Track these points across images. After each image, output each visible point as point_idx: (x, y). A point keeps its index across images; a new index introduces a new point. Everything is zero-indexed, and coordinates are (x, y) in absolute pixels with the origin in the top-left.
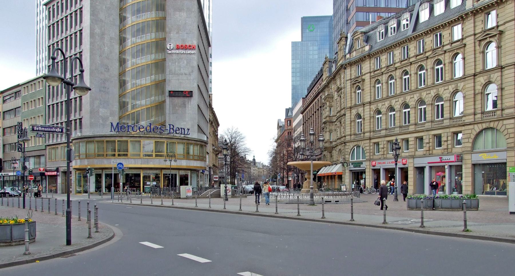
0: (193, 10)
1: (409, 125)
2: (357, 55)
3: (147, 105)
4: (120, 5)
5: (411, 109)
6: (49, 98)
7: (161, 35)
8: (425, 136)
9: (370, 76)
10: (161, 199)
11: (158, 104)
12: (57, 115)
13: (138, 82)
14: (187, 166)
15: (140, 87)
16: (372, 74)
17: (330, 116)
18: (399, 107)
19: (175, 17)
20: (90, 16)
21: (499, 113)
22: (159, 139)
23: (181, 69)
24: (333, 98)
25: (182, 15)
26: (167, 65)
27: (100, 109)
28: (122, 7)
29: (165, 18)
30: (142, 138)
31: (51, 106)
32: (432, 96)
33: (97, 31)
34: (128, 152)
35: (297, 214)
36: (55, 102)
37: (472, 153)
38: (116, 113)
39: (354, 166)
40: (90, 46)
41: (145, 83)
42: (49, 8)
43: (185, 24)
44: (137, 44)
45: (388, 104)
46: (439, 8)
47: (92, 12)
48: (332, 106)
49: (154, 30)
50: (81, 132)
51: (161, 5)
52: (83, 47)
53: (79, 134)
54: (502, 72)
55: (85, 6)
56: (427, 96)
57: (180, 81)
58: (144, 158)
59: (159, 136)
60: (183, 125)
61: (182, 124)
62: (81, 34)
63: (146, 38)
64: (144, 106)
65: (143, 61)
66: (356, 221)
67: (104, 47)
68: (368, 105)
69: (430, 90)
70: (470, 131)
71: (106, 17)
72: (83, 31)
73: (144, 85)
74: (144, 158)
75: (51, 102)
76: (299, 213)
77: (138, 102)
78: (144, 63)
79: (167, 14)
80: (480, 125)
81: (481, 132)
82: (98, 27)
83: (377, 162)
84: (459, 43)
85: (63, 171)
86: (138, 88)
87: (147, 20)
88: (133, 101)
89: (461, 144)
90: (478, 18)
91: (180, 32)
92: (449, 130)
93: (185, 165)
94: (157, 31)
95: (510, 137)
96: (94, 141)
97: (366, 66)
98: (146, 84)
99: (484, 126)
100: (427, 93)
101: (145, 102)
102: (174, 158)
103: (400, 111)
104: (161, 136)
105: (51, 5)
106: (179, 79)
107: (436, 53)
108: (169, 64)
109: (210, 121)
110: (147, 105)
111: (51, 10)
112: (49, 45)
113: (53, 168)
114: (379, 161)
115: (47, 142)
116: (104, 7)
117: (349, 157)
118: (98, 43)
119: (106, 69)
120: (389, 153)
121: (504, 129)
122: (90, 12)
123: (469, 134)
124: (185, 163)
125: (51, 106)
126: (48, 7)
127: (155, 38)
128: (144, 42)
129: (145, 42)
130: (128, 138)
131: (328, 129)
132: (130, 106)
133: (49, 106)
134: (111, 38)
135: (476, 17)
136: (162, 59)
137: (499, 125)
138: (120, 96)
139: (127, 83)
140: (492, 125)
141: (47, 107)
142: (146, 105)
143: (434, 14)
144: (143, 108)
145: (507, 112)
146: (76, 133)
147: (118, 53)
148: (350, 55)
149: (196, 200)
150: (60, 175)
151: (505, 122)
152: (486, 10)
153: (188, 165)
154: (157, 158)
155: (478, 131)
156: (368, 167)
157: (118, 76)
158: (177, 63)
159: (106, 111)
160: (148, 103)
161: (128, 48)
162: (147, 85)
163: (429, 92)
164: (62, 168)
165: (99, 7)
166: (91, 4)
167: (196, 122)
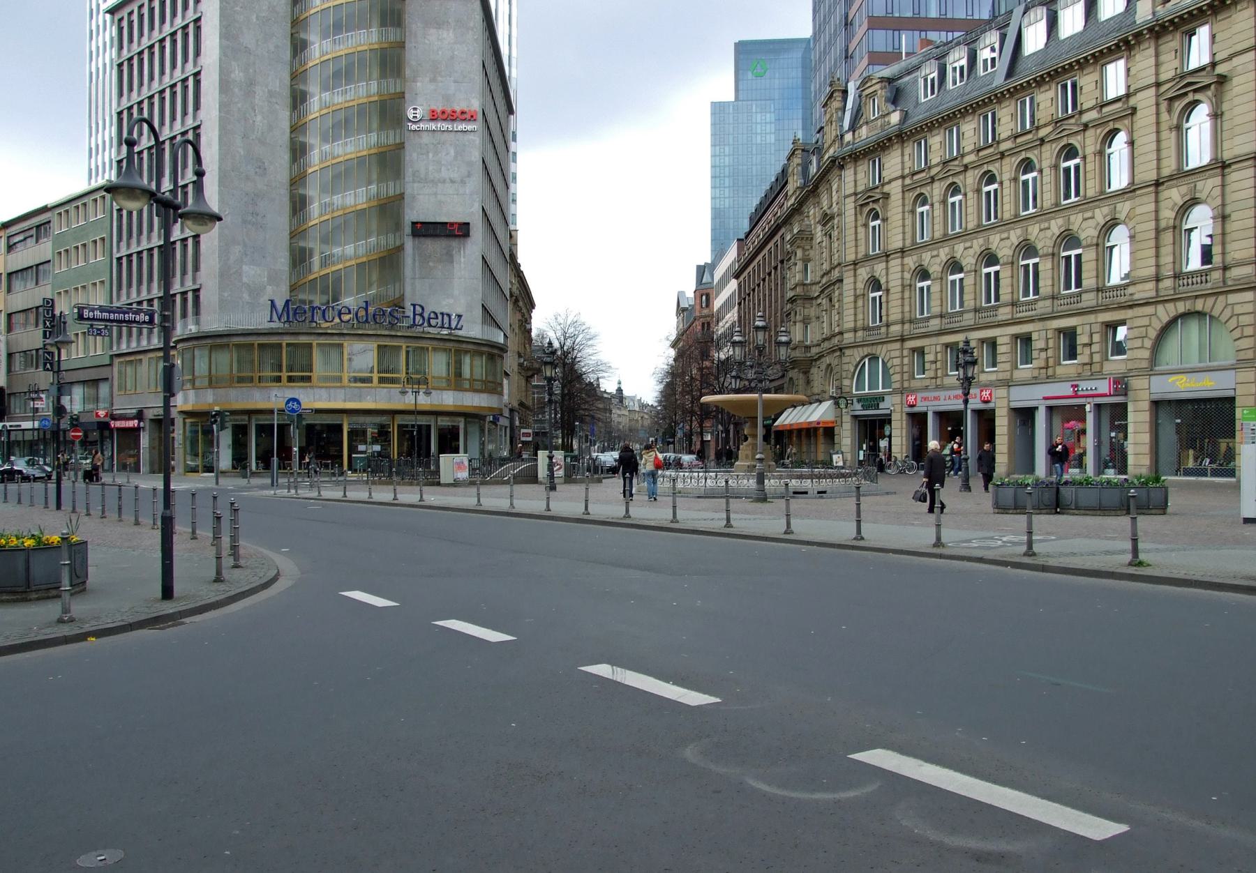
0: (472, 24)
1: (999, 307)
2: (870, 134)
3: (359, 258)
4: (293, 11)
5: (1001, 265)
7: (392, 86)
8: (1037, 333)
9: (903, 186)
13: (337, 199)
15: (341, 213)
16: (908, 181)
17: (804, 285)
19: (427, 41)
21: (1217, 275)
22: (388, 339)
24: (812, 239)
26: (407, 158)
28: (297, 18)
29: (401, 45)
30: (347, 338)
33: (237, 75)
36: (134, 249)
37: (1150, 375)
39: (862, 406)
40: (220, 112)
42: (121, 20)
43: (452, 58)
44: (334, 108)
46: (1072, 21)
47: (224, 30)
48: (809, 260)
49: (376, 74)
50: (197, 323)
52: (202, 114)
53: (193, 328)
54: (1223, 176)
55: (208, 14)
56: (1042, 235)
58: (351, 387)
59: (387, 333)
60: (446, 305)
62: (197, 83)
64: (351, 259)
67: (253, 114)
70: (1145, 321)
71: (257, 41)
72: (203, 76)
74: (351, 387)
76: (728, 519)
77: (337, 250)
78: (351, 153)
80: (1170, 306)
81: (1172, 322)
82: (238, 65)
83: (920, 395)
84: (1119, 105)
85: (153, 418)
86: (336, 214)
87: (359, 49)
88: (325, 247)
90: (1165, 43)
91: (439, 79)
92: (1096, 318)
93: (451, 404)
94: (383, 75)
95: (1245, 335)
98: (356, 206)
99: (1181, 307)
100: (1042, 227)
102: (425, 387)
103: (976, 271)
105: (124, 13)
106: (436, 194)
109: (511, 295)
111: (125, 24)
113: (129, 411)
114: (926, 394)
115: (115, 348)
116: (254, 18)
117: (852, 384)
118: (239, 105)
119: (257, 170)
121: (1230, 315)
122: (220, 29)
123: (1144, 329)
124: (452, 399)
126: (117, 17)
128: (351, 104)
129: (354, 103)
130: (312, 338)
131: (800, 315)
132: (316, 259)
133: (119, 259)
134: (271, 94)
136: (396, 144)
137: (1217, 306)
140: (1199, 305)
141: (115, 261)
142: (356, 257)
146: (185, 326)
147: (289, 131)
148: (854, 134)
149: (478, 490)
150: (147, 427)
151: (1232, 298)
152: (1185, 24)
153: (459, 404)
154: (382, 385)
155: (1165, 319)
156: (898, 408)
160: (361, 251)
161: (313, 116)
162: (359, 208)
163: (1046, 225)
164: (151, 410)
165: (242, 17)
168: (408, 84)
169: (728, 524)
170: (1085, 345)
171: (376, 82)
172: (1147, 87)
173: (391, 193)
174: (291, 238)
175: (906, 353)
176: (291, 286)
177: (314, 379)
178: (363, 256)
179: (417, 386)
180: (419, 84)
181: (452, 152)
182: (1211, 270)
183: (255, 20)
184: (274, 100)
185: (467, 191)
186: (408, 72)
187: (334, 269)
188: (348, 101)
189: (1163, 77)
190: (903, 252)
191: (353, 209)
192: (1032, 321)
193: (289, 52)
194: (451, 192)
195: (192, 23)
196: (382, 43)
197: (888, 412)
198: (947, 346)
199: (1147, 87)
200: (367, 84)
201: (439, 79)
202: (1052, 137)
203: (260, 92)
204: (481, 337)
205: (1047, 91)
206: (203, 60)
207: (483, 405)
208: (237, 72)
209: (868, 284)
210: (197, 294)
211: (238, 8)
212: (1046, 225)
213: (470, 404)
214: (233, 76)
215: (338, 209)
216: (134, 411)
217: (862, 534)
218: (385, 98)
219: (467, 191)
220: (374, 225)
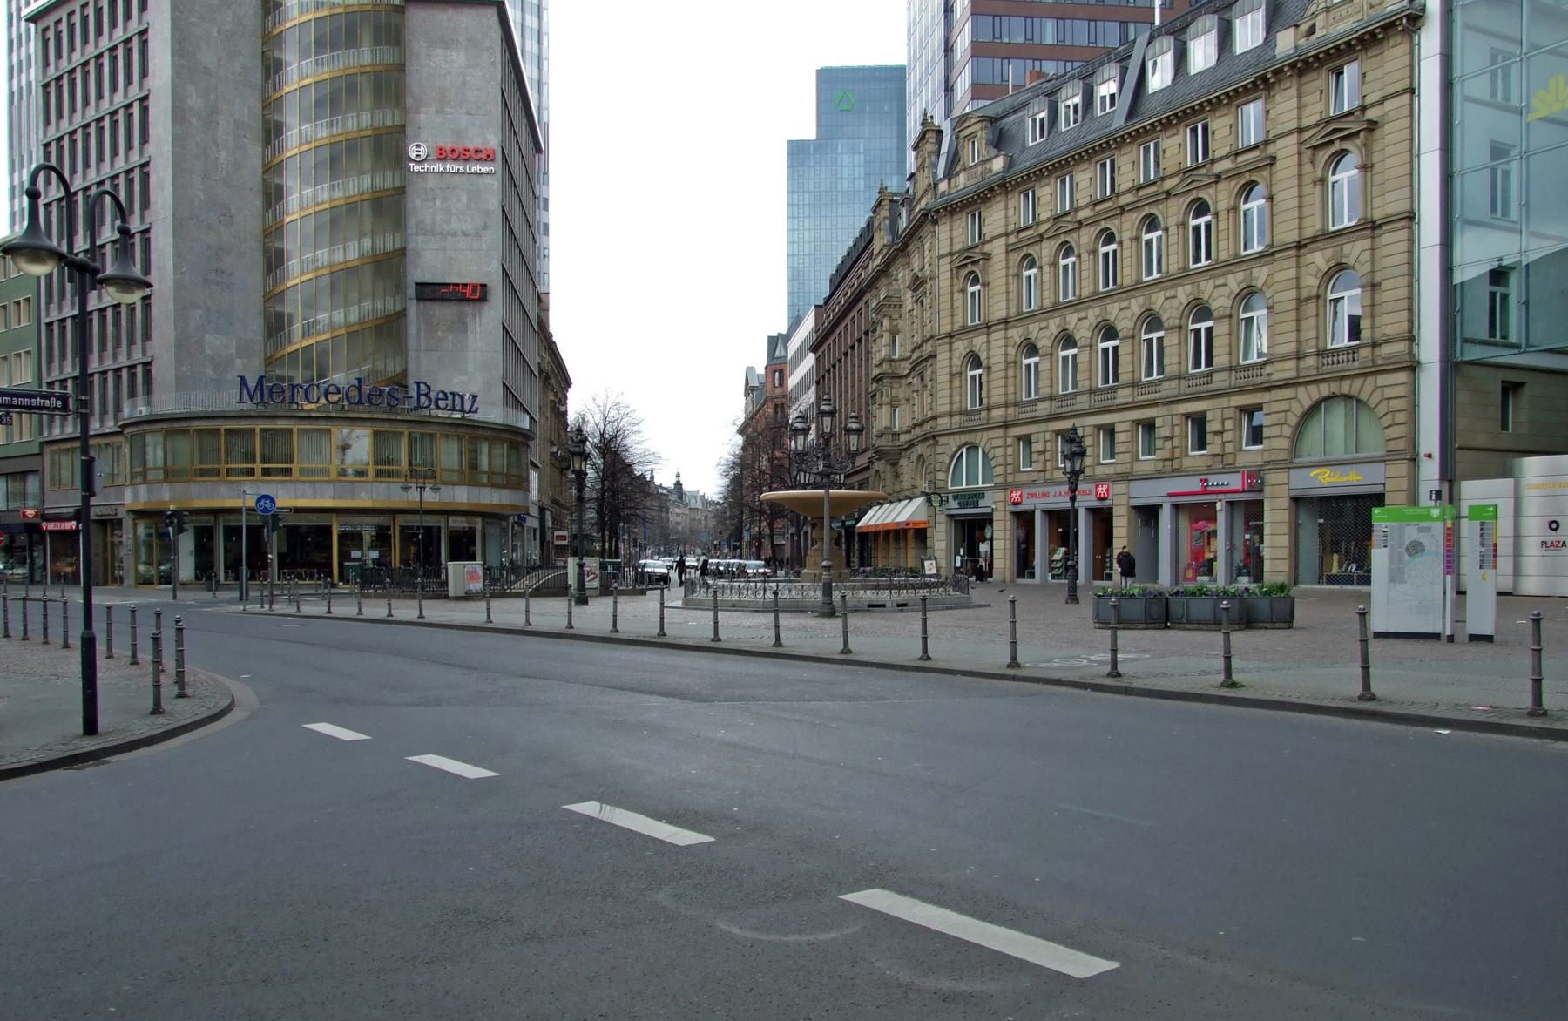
9: (1007, 245)
14: (470, 504)
16: (1012, 239)
17: (893, 360)
18: (1228, 303)
26: (409, 206)
30: (335, 423)
32: (1232, 292)
39: (959, 504)
42: (46, 30)
45: (1328, 261)
50: (149, 403)
53: (143, 410)
54: (1298, 256)
56: (1167, 304)
67: (215, 149)
68: (1000, 330)
69: (1128, 298)
70: (1284, 406)
71: (219, 60)
80: (1313, 389)
81: (1314, 409)
83: (1026, 491)
89: (1261, 443)
91: (448, 110)
92: (1229, 401)
93: (465, 501)
95: (1396, 422)
97: (997, 217)
99: (1325, 390)
101: (342, 315)
103: (1091, 346)
105: (50, 21)
107: (1193, 181)
109: (541, 371)
111: (51, 35)
113: (65, 511)
120: (1022, 469)
124: (465, 496)
126: (42, 25)
131: (887, 396)
133: (50, 325)
135: (1304, 80)
136: (394, 189)
141: (43, 327)
143: (1231, 46)
145: (995, 413)
146: (134, 407)
147: (260, 170)
148: (949, 183)
153: (476, 501)
155: (1307, 403)
156: (1000, 506)
163: (1172, 293)
170: (1216, 433)
172: (1288, 133)
175: (1009, 441)
180: (422, 116)
181: (465, 199)
182: (1358, 347)
189: (1306, 122)
190: (1006, 322)
192: (1156, 405)
197: (989, 510)
198: (1057, 433)
199: (1288, 133)
201: (448, 110)
202: (1180, 190)
205: (1174, 135)
208: (194, 98)
209: (1323, 285)
212: (1172, 293)
214: (189, 102)
215: (323, 267)
216: (72, 510)
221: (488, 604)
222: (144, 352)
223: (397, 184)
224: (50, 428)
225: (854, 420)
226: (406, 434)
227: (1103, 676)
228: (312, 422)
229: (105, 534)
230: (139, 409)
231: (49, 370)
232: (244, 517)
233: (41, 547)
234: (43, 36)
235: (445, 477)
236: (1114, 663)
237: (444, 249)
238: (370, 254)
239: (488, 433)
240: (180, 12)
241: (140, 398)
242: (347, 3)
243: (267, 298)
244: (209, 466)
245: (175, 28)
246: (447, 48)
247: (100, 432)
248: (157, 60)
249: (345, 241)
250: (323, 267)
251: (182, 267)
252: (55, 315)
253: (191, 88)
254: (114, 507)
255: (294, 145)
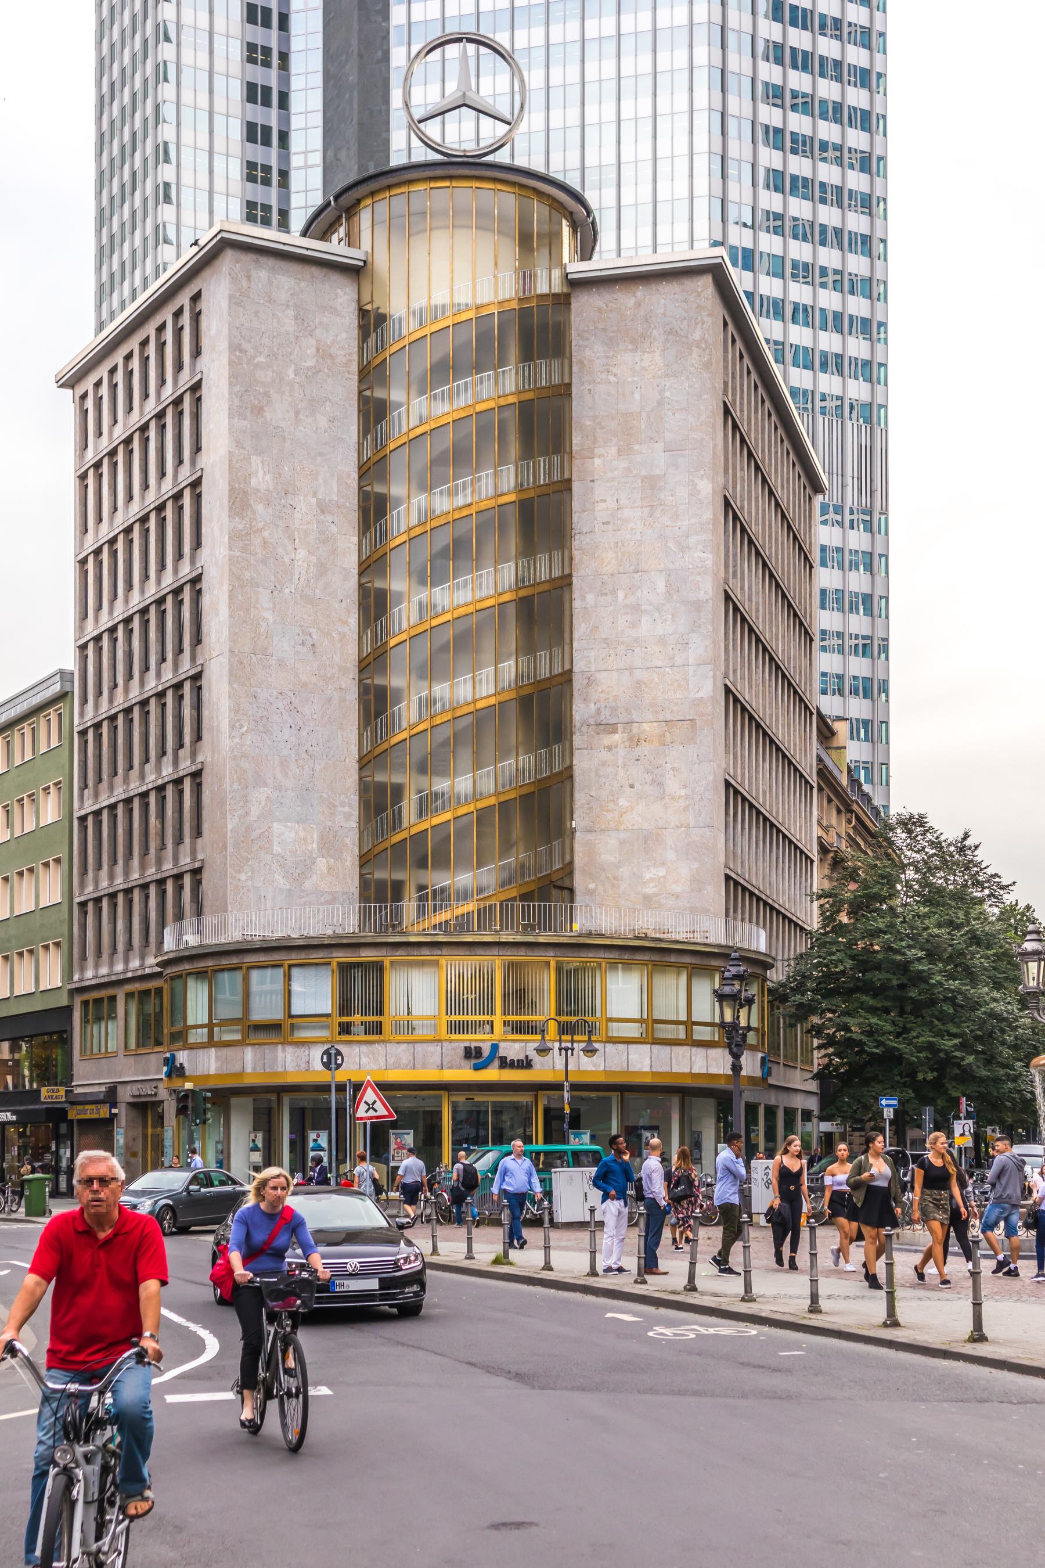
0: (697, 335)
3: (482, 798)
4: (361, 349)
6: (84, 786)
7: (543, 472)
10: (462, 1231)
11: (531, 789)
12: (114, 861)
13: (441, 690)
14: (654, 1074)
15: (448, 716)
19: (612, 378)
20: (231, 416)
22: (522, 951)
23: (643, 620)
25: (646, 364)
26: (577, 604)
27: (275, 825)
28: (369, 363)
29: (564, 391)
30: (445, 951)
31: (90, 819)
33: (261, 479)
34: (380, 1012)
35: (809, 1302)
36: (105, 801)
38: (348, 841)
40: (231, 549)
41: (469, 698)
42: (84, 397)
43: (660, 403)
44: (435, 524)
47: (237, 402)
49: (514, 448)
50: (199, 932)
51: (544, 327)
52: (205, 554)
53: (191, 939)
55: (211, 376)
57: (638, 673)
58: (451, 1041)
59: (519, 938)
60: (652, 880)
61: (648, 876)
62: (197, 498)
63: (473, 492)
64: (467, 802)
65: (464, 596)
66: (994, 1342)
67: (290, 547)
71: (297, 413)
72: (205, 488)
73: (468, 704)
74: (451, 1041)
75: (91, 802)
76: (814, 1298)
77: (441, 785)
78: (466, 605)
79: (575, 369)
82: (263, 463)
85: (131, 1100)
86: (438, 720)
87: (479, 408)
88: (424, 781)
91: (637, 447)
93: (647, 1069)
94: (527, 452)
96: (206, 972)
98: (475, 701)
101: (470, 782)
102: (539, 1037)
104: (530, 939)
105: (88, 384)
106: (631, 669)
108: (584, 598)
109: (824, 849)
110: (482, 798)
111: (90, 403)
112: (81, 557)
113: (96, 1089)
115: (76, 977)
116: (290, 373)
118: (266, 534)
119: (299, 648)
122: (231, 400)
124: (647, 1062)
125: (90, 819)
126: (80, 390)
127: (520, 489)
128: (465, 513)
129: (472, 510)
130: (383, 952)
132: (409, 806)
133: (83, 819)
134: (323, 508)
136: (552, 580)
138: (365, 762)
139: (397, 701)
141: (76, 823)
142: (477, 796)
144: (462, 811)
146: (180, 934)
147: (356, 572)
149: (469, 1233)
150: (123, 1120)
153: (665, 1069)
154: (454, 1037)
157: (354, 672)
158: (621, 595)
159: (302, 834)
160: (487, 785)
161: (398, 541)
162: (481, 705)
164: (129, 1087)
165: (269, 373)
166: (231, 363)
167: (716, 862)
168: (576, 463)
169: (814, 1308)
171: (512, 467)
173: (544, 673)
174: (361, 769)
176: (361, 857)
177: (387, 1028)
178: (490, 796)
179: (569, 1037)
180: (597, 461)
181: (661, 587)
183: (292, 376)
184: (330, 518)
185: (691, 661)
186: (577, 440)
187: (436, 821)
188: (461, 508)
191: (471, 708)
193: (355, 428)
194: (660, 664)
195: (188, 393)
196: (524, 391)
200: (495, 473)
201: (637, 447)
203: (304, 507)
204: (723, 942)
206: (205, 459)
207: (713, 1070)
208: (261, 474)
210: (198, 877)
211: (261, 359)
213: (687, 1070)
214: (253, 482)
215: (443, 712)
216: (103, 1089)
217: (985, 1330)
218: (531, 494)
219: (691, 661)
220: (513, 735)
221: (469, 1233)
222: (193, 852)
223: (557, 573)
224: (82, 970)
225: (1034, 936)
226: (553, 964)
227: (875, 1326)
228: (411, 951)
229: (145, 1127)
230: (185, 938)
231: (82, 885)
232: (566, 1095)
233: (69, 1143)
234: (82, 405)
235: (619, 1030)
236: (814, 1298)
237: (631, 669)
238: (513, 685)
239: (687, 959)
240: (241, 351)
241: (189, 922)
242: (479, 302)
243: (365, 761)
244: (470, 1018)
245: (234, 377)
246: (635, 350)
247: (139, 973)
248: (212, 426)
249: (477, 666)
250: (443, 712)
251: (241, 726)
252: (89, 807)
253: (256, 461)
254: (154, 1084)
255: (402, 530)
